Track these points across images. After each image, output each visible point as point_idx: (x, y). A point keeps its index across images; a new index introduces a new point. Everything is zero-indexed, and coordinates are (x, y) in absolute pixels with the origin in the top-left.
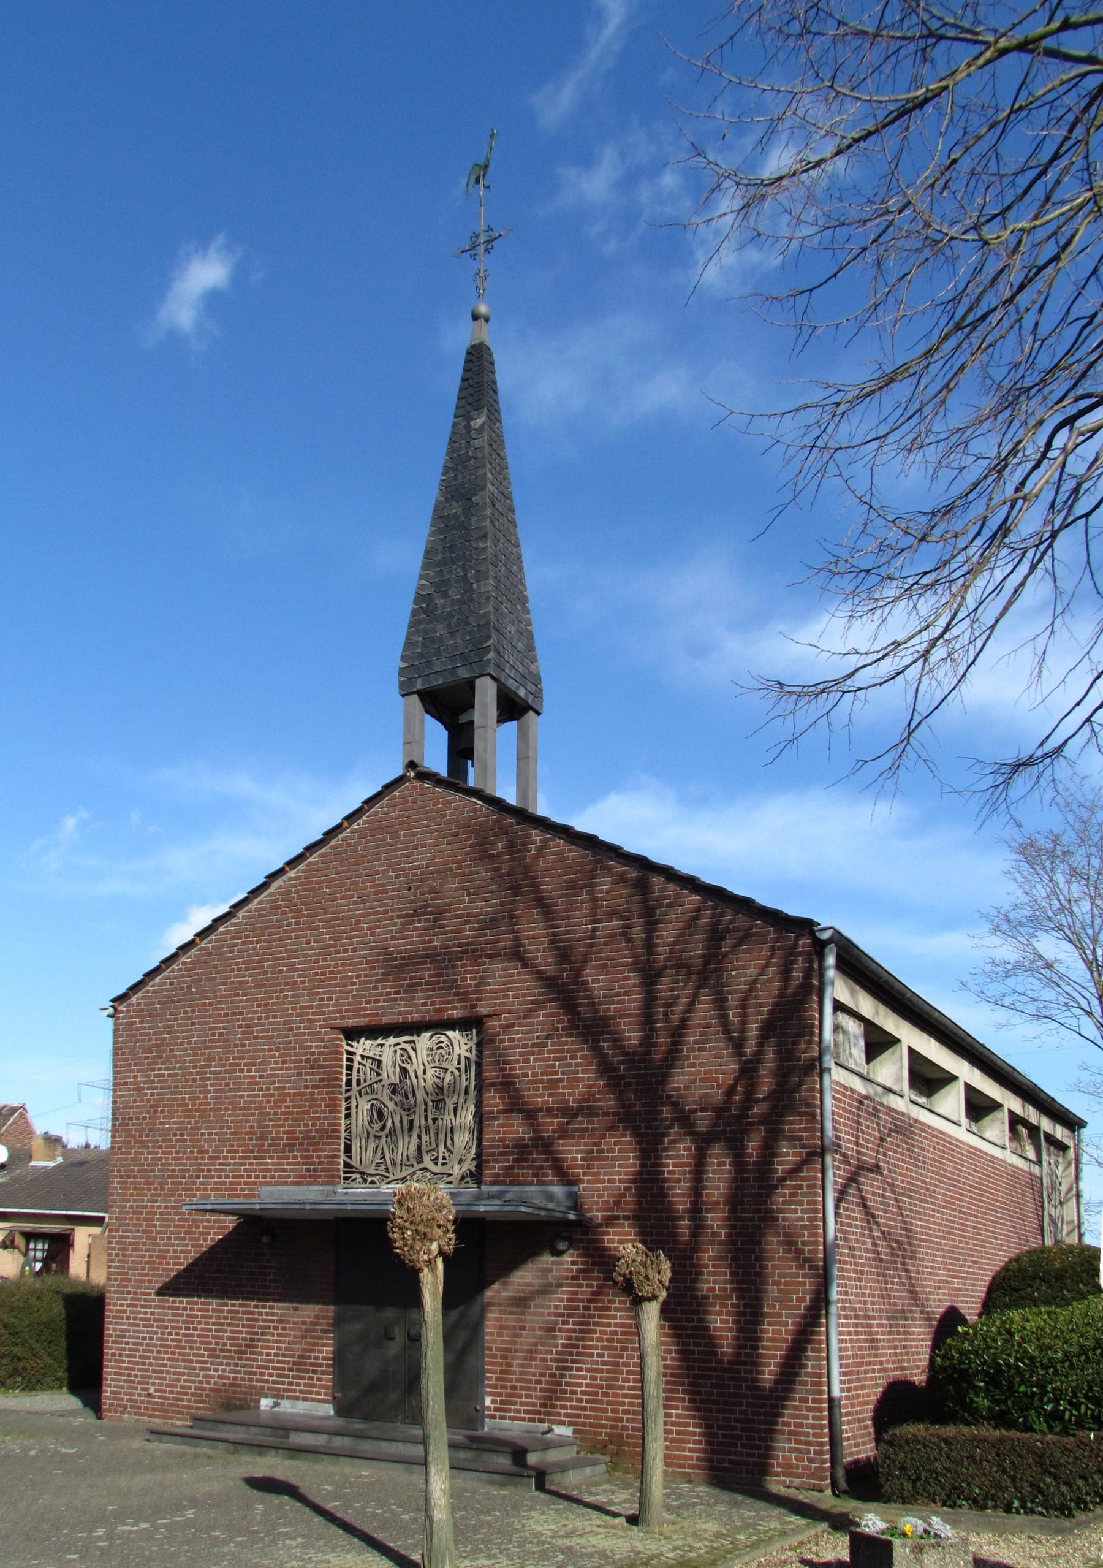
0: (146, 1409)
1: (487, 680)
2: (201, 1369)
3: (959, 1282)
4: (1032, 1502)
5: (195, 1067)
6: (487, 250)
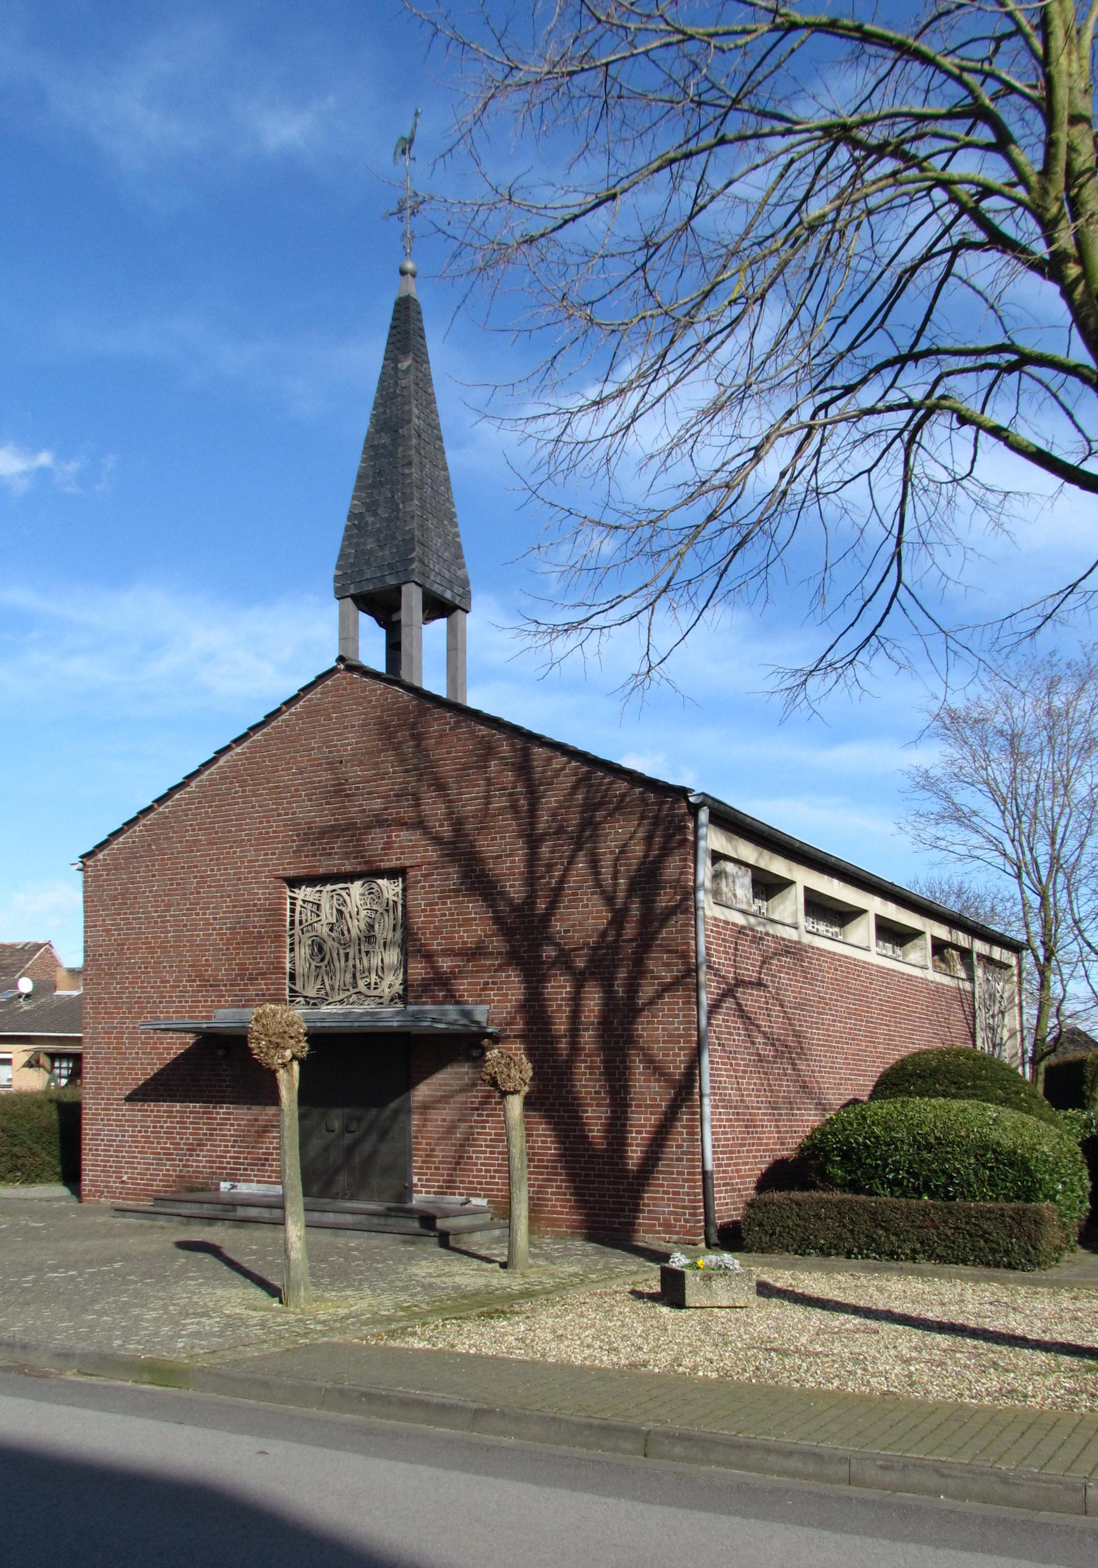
0: (121, 1193)
1: (413, 586)
2: (168, 1160)
3: (844, 1075)
4: (868, 1249)
5: (156, 912)
6: (413, 213)
